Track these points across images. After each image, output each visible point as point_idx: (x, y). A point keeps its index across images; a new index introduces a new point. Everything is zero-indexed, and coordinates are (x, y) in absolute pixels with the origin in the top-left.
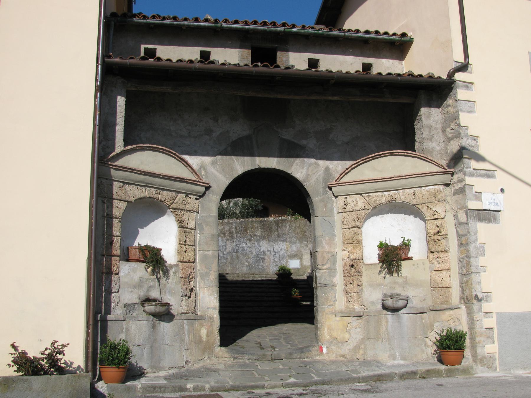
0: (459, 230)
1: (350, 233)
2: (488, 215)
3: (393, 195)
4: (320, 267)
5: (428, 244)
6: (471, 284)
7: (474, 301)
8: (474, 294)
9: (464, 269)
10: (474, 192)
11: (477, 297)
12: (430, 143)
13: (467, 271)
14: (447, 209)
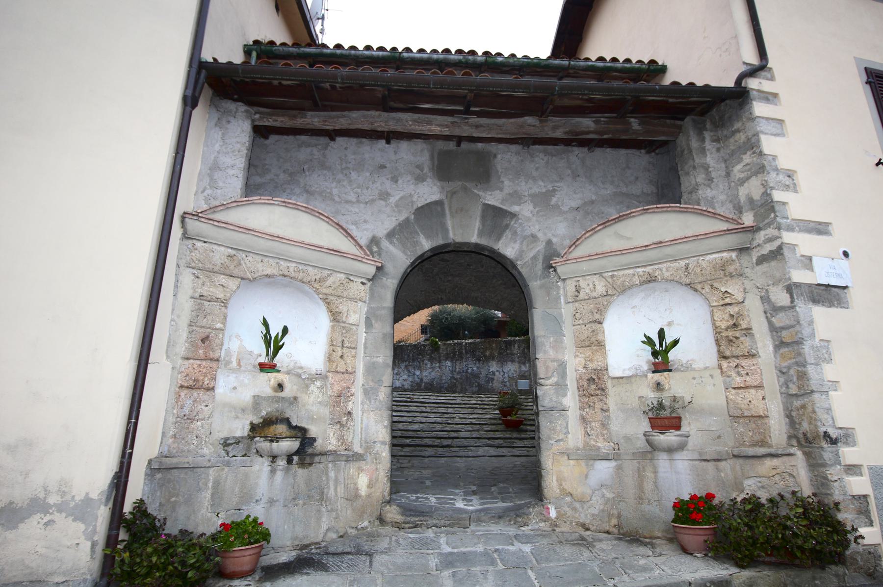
0: (773, 319)
1: (586, 332)
2: (829, 295)
3: (651, 271)
4: (542, 381)
5: (717, 342)
6: (814, 412)
7: (824, 444)
8: (822, 430)
9: (791, 385)
10: (798, 255)
11: (829, 436)
12: (709, 190)
13: (799, 388)
14: (748, 287)
